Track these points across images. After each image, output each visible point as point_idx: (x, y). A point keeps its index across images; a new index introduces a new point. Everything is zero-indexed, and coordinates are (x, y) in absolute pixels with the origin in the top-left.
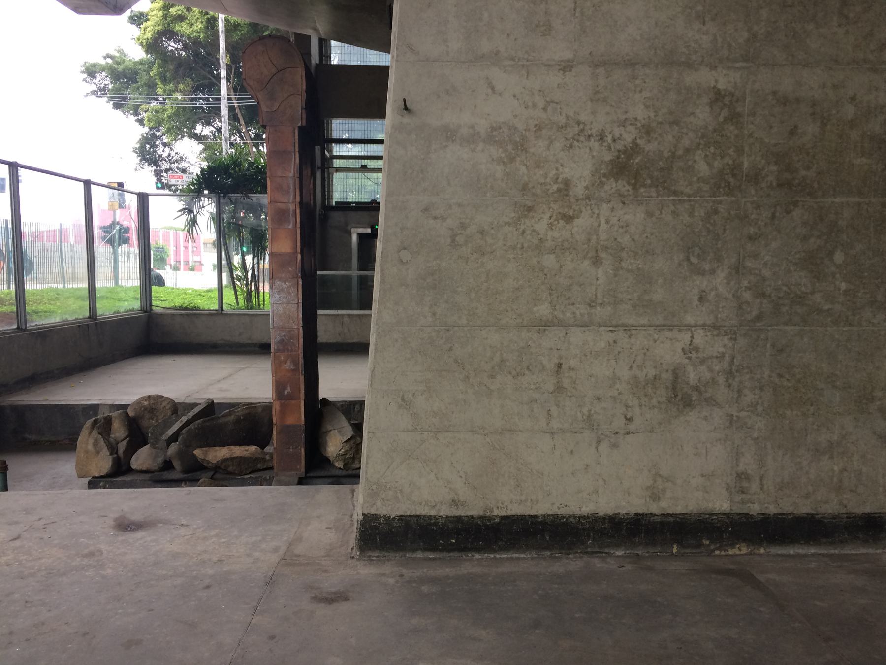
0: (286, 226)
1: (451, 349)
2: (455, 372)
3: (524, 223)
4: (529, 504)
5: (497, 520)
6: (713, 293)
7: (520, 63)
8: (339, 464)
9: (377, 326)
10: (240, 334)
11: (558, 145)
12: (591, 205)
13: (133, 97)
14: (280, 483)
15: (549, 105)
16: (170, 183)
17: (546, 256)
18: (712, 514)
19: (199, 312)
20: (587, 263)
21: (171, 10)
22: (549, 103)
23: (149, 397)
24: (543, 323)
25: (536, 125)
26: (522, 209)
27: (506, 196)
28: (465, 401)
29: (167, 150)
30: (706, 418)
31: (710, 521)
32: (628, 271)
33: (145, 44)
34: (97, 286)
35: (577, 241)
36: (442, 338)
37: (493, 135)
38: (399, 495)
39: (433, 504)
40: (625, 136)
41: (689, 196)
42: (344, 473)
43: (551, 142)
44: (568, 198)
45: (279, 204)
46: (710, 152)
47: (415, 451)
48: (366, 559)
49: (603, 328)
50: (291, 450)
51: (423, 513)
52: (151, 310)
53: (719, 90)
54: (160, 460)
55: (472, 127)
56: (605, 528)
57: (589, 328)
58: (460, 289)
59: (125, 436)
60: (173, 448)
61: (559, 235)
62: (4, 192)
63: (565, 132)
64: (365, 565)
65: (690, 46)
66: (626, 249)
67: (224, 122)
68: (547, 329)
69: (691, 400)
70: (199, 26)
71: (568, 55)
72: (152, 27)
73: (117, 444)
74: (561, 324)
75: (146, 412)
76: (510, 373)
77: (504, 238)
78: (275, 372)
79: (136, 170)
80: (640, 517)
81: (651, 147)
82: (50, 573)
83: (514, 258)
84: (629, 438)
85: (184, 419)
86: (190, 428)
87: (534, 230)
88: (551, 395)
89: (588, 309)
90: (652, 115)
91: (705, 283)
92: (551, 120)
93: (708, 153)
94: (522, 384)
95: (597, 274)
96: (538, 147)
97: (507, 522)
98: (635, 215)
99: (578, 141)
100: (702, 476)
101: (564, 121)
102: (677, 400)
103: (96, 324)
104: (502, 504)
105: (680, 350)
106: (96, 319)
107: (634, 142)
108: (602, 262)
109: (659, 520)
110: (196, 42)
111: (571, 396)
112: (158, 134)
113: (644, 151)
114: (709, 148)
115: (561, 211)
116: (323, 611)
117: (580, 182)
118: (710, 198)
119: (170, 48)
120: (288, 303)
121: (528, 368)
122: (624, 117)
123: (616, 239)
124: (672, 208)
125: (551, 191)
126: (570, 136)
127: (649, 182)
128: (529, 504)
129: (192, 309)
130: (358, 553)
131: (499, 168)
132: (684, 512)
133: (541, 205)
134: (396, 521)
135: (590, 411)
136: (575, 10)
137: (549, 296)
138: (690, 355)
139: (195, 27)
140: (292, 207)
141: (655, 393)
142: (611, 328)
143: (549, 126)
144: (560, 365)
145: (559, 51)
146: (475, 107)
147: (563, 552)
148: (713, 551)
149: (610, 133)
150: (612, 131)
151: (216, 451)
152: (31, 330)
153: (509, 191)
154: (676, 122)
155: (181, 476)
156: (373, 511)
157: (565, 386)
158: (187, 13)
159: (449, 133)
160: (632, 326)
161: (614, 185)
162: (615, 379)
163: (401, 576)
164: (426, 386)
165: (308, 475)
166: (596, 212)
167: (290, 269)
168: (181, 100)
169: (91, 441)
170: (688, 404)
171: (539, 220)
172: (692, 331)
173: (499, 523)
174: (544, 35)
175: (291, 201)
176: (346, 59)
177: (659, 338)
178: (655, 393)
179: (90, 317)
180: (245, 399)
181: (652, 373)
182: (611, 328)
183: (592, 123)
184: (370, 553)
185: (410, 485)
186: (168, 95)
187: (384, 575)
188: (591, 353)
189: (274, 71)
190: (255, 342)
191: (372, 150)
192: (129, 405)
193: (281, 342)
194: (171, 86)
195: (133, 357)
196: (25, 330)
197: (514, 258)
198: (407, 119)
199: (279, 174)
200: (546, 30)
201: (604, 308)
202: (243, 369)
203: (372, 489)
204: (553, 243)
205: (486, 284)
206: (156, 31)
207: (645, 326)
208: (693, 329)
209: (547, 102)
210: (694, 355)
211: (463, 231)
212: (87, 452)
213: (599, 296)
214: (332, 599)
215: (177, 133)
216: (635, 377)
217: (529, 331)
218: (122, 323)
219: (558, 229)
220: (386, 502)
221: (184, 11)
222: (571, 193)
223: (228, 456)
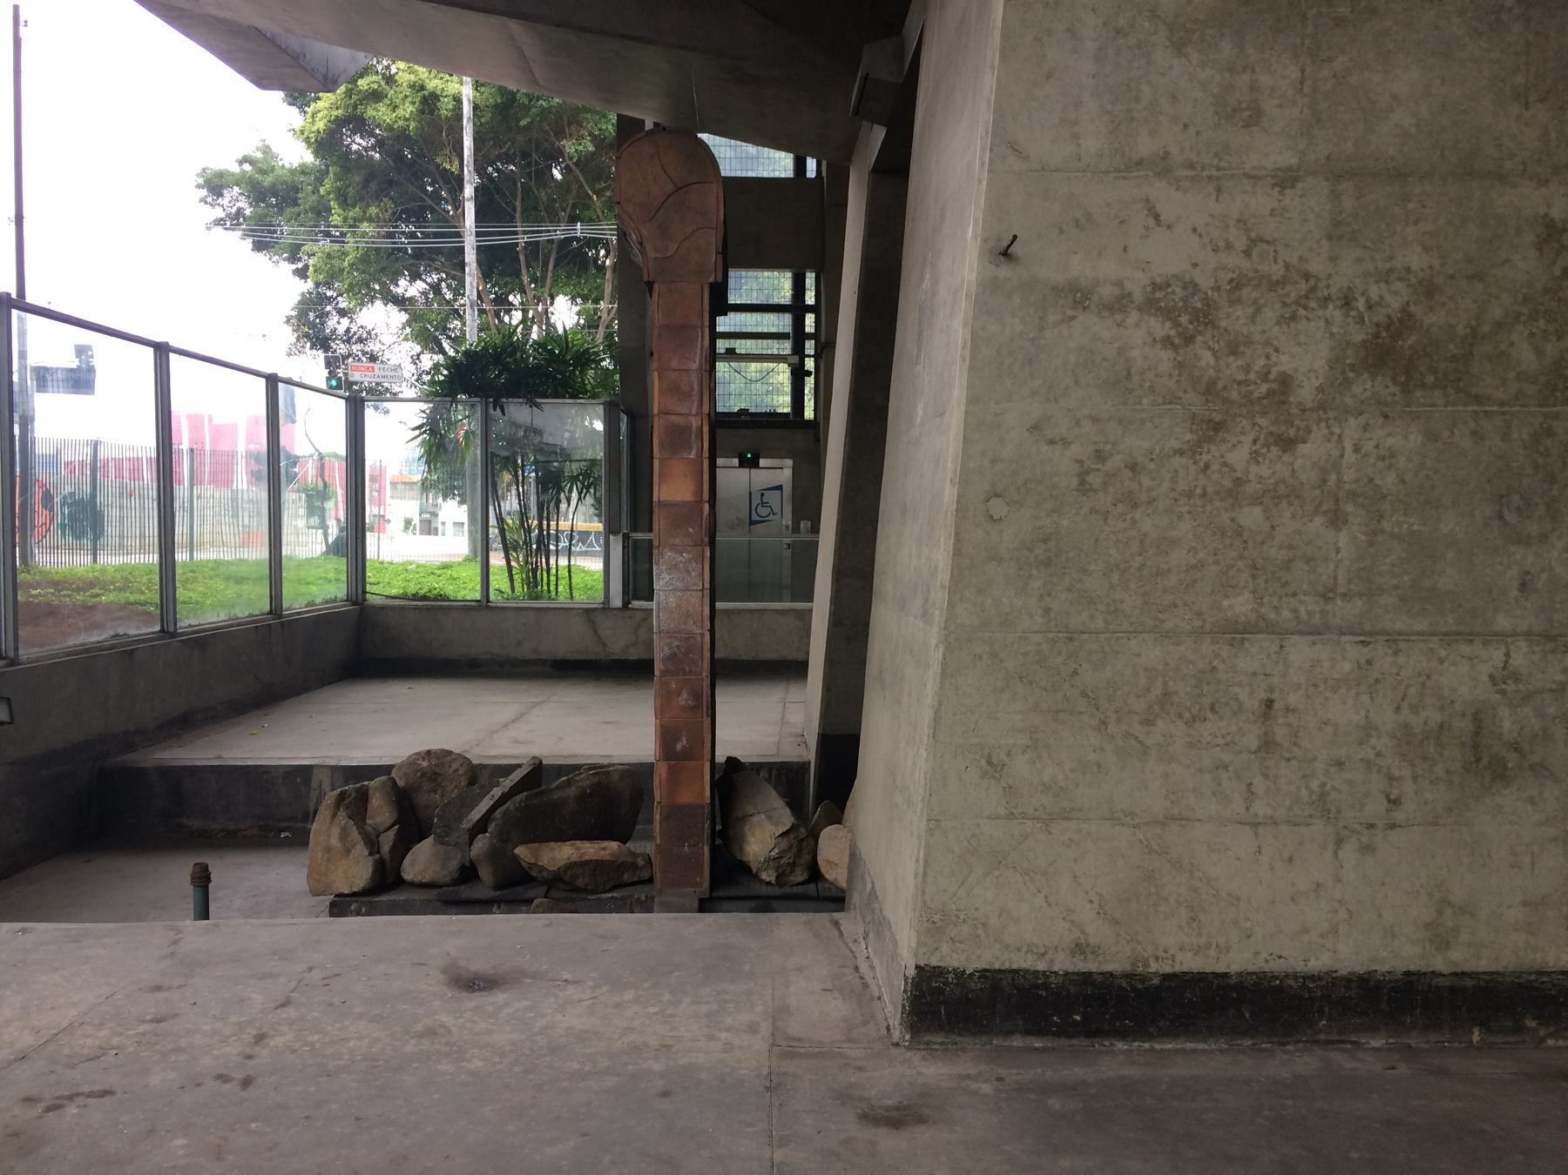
1: (1075, 673)
2: (1081, 713)
3: (1209, 451)
4: (1212, 953)
5: (1156, 981)
6: (1545, 576)
7: (1204, 173)
8: (768, 876)
9: (947, 632)
11: (1269, 315)
12: (1329, 419)
13: (286, 230)
14: (667, 908)
15: (1255, 246)
16: (351, 379)
17: (1246, 510)
18: (1541, 973)
19: (446, 603)
20: (1319, 521)
21: (360, 82)
22: (1253, 242)
23: (429, 752)
24: (1241, 628)
25: (1231, 281)
26: (1204, 426)
27: (1176, 404)
28: (1099, 766)
29: (345, 322)
30: (1531, 800)
31: (1536, 984)
32: (1393, 536)
33: (313, 140)
34: (284, 553)
35: (1302, 484)
36: (1060, 653)
37: (1156, 301)
38: (980, 931)
39: (1042, 950)
40: (1389, 299)
41: (1502, 404)
42: (777, 891)
43: (1258, 310)
44: (1286, 407)
45: (673, 417)
46: (1538, 327)
47: (1009, 854)
48: (922, 1047)
49: (1348, 638)
50: (686, 849)
51: (1025, 965)
52: (365, 600)
53: (1552, 220)
54: (454, 865)
55: (1119, 283)
56: (1351, 998)
57: (1322, 637)
58: (1093, 567)
60: (481, 844)
61: (1271, 471)
62: (93, 393)
63: (1282, 292)
64: (924, 1059)
65: (1501, 145)
66: (1390, 498)
67: (470, 275)
68: (1247, 639)
69: (1505, 768)
70: (408, 109)
71: (1288, 159)
72: (326, 112)
73: (378, 836)
74: (1272, 629)
75: (425, 779)
76: (1180, 716)
77: (1172, 478)
78: (660, 712)
79: (290, 355)
80: (1413, 978)
81: (1435, 318)
82: (375, 1067)
83: (1190, 512)
84: (1394, 835)
85: (497, 792)
86: (507, 809)
87: (1225, 464)
88: (1253, 756)
89: (1322, 602)
90: (1436, 263)
91: (1531, 558)
93: (1534, 330)
94: (1202, 735)
95: (1338, 541)
96: (1236, 319)
97: (1173, 984)
98: (1406, 438)
99: (1306, 308)
100: (1525, 903)
101: (1282, 272)
102: (1480, 766)
103: (282, 623)
104: (1166, 952)
105: (1485, 679)
106: (280, 616)
107: (1404, 309)
108: (1347, 521)
109: (1447, 984)
110: (402, 137)
111: (1289, 760)
112: (329, 293)
113: (1421, 326)
114: (1537, 321)
115: (1272, 429)
116: (889, 1142)
117: (1309, 379)
118: (1539, 409)
119: (354, 147)
120: (686, 589)
121: (1212, 709)
122: (1388, 266)
123: (1371, 480)
124: (1472, 425)
125: (1256, 395)
127: (1430, 379)
128: (1212, 953)
129: (435, 599)
130: (908, 1037)
131: (1166, 356)
132: (1493, 968)
133: (1238, 420)
134: (975, 979)
135: (1323, 785)
136: (1301, 83)
137: (1250, 580)
138: (1504, 686)
139: (400, 112)
140: (695, 422)
141: (1441, 755)
142: (1362, 638)
143: (1253, 282)
144: (1269, 703)
145: (1272, 152)
146: (1125, 249)
147: (1275, 1040)
148: (1543, 1040)
149: (1363, 294)
150: (1366, 290)
151: (552, 850)
152: (183, 634)
153: (1181, 395)
154: (1478, 277)
155: (491, 894)
156: (934, 962)
157: (1278, 739)
158: (387, 87)
159: (1079, 295)
160: (1400, 634)
161: (1369, 385)
162: (1368, 729)
163: (1000, 1079)
164: (1031, 738)
165: (714, 894)
166: (1337, 430)
167: (690, 530)
168: (373, 237)
169: (336, 831)
170: (1500, 774)
171: (1234, 445)
172: (1506, 643)
173: (1158, 988)
174: (1247, 126)
177: (1448, 655)
178: (1441, 755)
179: (270, 613)
180: (565, 757)
181: (1436, 717)
182: (1362, 638)
183: (1330, 276)
184: (927, 1038)
185: (1000, 915)
186: (350, 226)
187: (968, 1076)
188: (1326, 682)
189: (670, 188)
190: (543, 657)
191: (733, 322)
192: (393, 766)
193: (672, 658)
194: (355, 212)
195: (347, 678)
196: (174, 635)
197: (1190, 512)
198: (1005, 271)
199: (674, 364)
200: (1250, 116)
201: (1349, 602)
202: (540, 703)
203: (933, 922)
204: (1259, 485)
206: (333, 118)
207: (1423, 635)
208: (1509, 640)
209: (1252, 240)
210: (1511, 687)
211: (1099, 466)
212: (328, 849)
213: (1341, 579)
214: (898, 1118)
215: (363, 293)
216: (1406, 727)
217: (1214, 642)
218: (320, 623)
219: (1267, 461)
220: (958, 945)
221: (383, 83)
223: (575, 858)
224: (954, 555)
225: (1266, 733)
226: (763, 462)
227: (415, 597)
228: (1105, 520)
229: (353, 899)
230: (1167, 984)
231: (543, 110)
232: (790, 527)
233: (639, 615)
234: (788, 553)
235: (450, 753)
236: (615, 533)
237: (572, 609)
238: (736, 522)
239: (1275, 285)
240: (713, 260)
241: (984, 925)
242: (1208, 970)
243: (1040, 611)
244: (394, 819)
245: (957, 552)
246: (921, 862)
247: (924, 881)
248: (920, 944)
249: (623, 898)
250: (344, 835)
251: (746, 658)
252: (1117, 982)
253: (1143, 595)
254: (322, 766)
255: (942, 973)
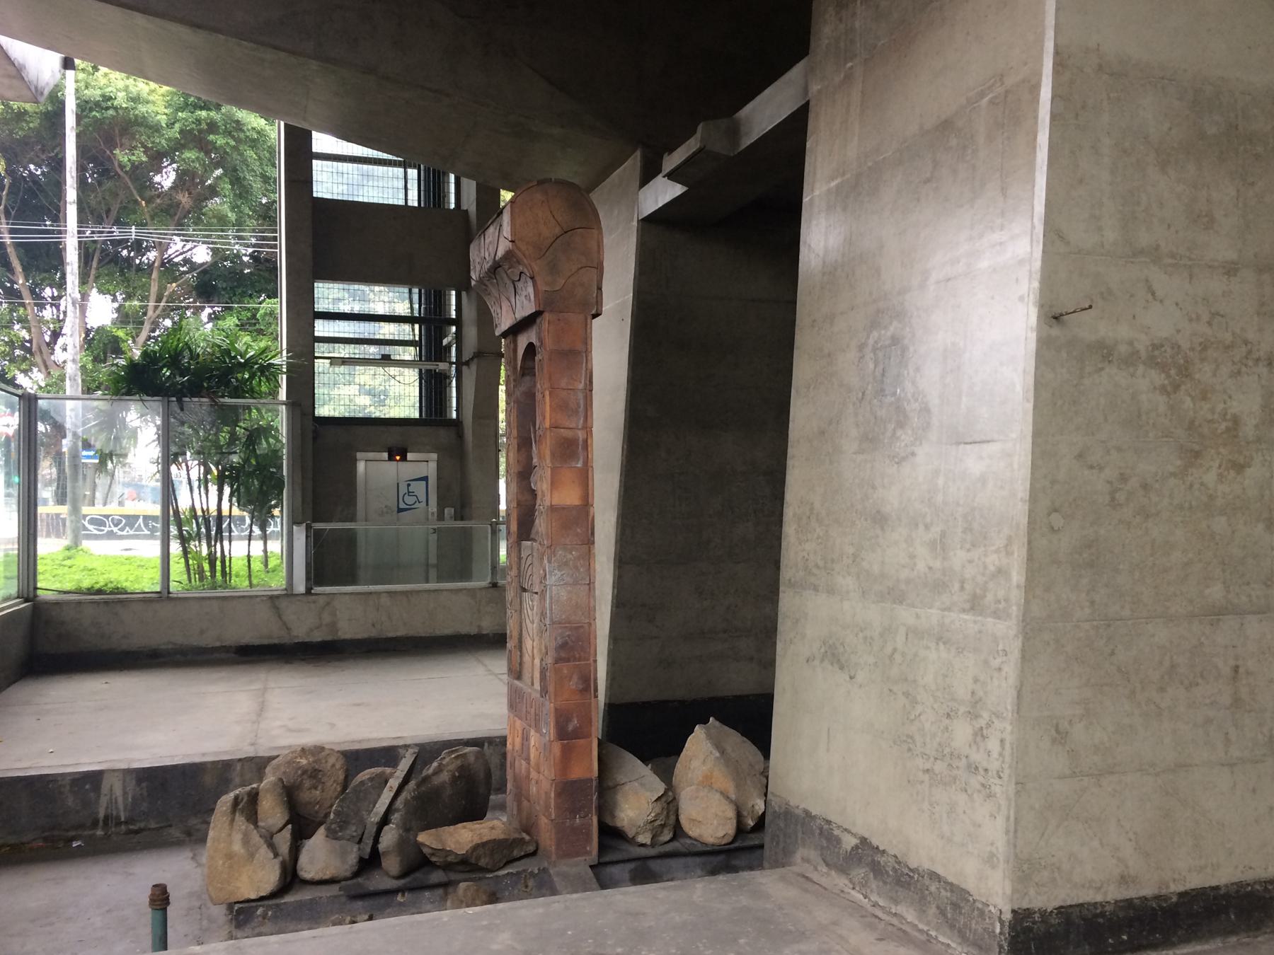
0: (573, 464)
5: (1174, 899)
7: (1181, 262)
10: (202, 632)
19: (125, 596)
20: (1261, 526)
25: (1201, 344)
38: (1056, 874)
39: (1099, 885)
42: (652, 852)
45: (562, 430)
50: (578, 821)
52: (36, 596)
55: (1131, 343)
58: (1121, 567)
59: (283, 822)
67: (72, 274)
71: (1231, 255)
75: (305, 777)
76: (1182, 683)
83: (1182, 522)
87: (1202, 484)
92: (1216, 338)
120: (575, 583)
121: (1202, 676)
125: (1219, 431)
126: (1237, 359)
129: (111, 593)
131: (1161, 400)
134: (1054, 916)
143: (1215, 346)
144: (1236, 669)
145: (1221, 249)
155: (390, 884)
156: (1025, 906)
165: (601, 860)
167: (579, 530)
169: (237, 837)
171: (1208, 469)
173: (1177, 904)
175: (580, 427)
176: (345, 192)
180: (360, 742)
185: (1070, 859)
189: (557, 230)
190: (227, 643)
197: (1182, 522)
198: (1056, 331)
205: (1151, 559)
212: (230, 856)
222: (1240, 434)
224: (1028, 560)
225: (1235, 693)
226: (410, 456)
227: (90, 591)
228: (1129, 529)
229: (259, 903)
230: (1182, 900)
231: (96, 120)
232: (436, 515)
233: (322, 600)
234: (435, 536)
235: (322, 749)
236: (298, 523)
237: (257, 596)
238: (385, 510)
239: (1228, 348)
240: (595, 295)
241: (1058, 869)
242: (1207, 886)
243: (1088, 604)
244: (287, 818)
245: (1030, 558)
246: (1012, 819)
247: (1016, 837)
248: (1014, 891)
249: (518, 873)
250: (246, 841)
251: (423, 635)
252: (1149, 903)
253: (1156, 587)
254: (114, 771)
255: (1030, 914)
